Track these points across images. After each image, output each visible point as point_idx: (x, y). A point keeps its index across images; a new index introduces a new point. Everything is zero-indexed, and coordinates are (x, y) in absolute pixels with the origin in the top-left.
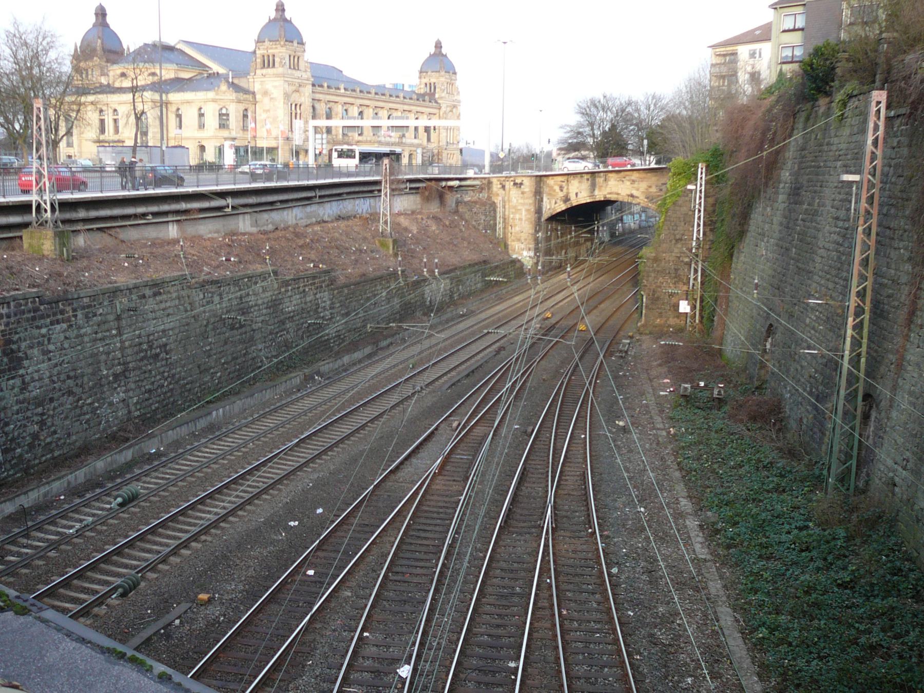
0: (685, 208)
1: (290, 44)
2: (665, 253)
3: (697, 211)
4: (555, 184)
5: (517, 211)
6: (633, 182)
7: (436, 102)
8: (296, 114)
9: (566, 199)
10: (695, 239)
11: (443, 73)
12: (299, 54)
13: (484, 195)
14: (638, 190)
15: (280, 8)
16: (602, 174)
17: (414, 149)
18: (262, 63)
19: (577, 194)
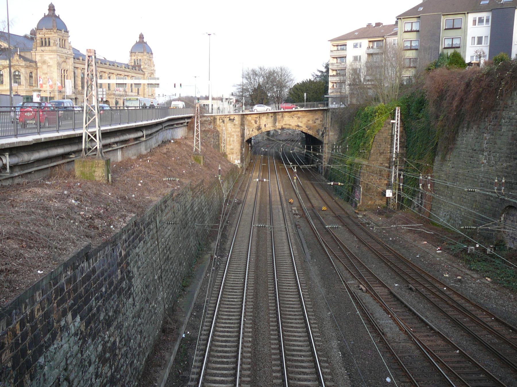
0: (385, 134)
1: (60, 32)
2: (374, 161)
3: (395, 135)
4: (252, 120)
5: (231, 136)
6: (299, 118)
7: (142, 71)
8: (64, 76)
9: (259, 128)
10: (394, 152)
11: (145, 53)
12: (65, 38)
13: (212, 126)
14: (301, 122)
15: (52, 8)
16: (280, 113)
17: (119, 97)
18: (41, 43)
19: (265, 125)
